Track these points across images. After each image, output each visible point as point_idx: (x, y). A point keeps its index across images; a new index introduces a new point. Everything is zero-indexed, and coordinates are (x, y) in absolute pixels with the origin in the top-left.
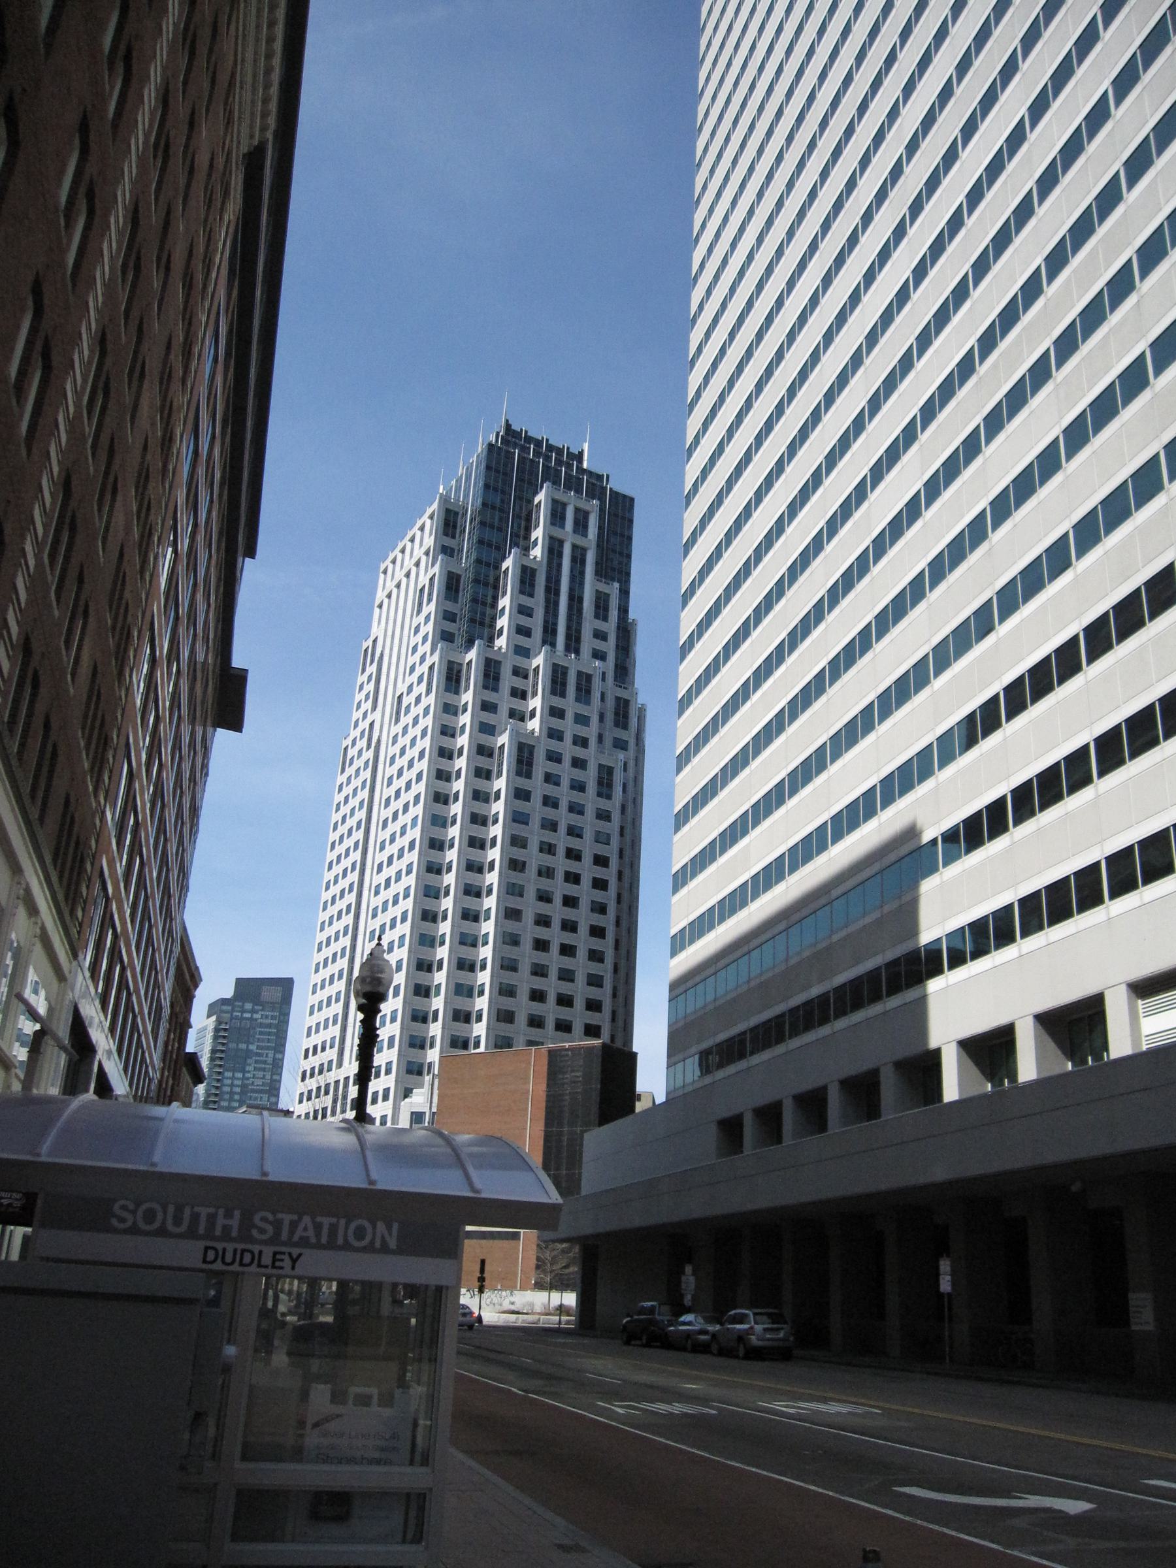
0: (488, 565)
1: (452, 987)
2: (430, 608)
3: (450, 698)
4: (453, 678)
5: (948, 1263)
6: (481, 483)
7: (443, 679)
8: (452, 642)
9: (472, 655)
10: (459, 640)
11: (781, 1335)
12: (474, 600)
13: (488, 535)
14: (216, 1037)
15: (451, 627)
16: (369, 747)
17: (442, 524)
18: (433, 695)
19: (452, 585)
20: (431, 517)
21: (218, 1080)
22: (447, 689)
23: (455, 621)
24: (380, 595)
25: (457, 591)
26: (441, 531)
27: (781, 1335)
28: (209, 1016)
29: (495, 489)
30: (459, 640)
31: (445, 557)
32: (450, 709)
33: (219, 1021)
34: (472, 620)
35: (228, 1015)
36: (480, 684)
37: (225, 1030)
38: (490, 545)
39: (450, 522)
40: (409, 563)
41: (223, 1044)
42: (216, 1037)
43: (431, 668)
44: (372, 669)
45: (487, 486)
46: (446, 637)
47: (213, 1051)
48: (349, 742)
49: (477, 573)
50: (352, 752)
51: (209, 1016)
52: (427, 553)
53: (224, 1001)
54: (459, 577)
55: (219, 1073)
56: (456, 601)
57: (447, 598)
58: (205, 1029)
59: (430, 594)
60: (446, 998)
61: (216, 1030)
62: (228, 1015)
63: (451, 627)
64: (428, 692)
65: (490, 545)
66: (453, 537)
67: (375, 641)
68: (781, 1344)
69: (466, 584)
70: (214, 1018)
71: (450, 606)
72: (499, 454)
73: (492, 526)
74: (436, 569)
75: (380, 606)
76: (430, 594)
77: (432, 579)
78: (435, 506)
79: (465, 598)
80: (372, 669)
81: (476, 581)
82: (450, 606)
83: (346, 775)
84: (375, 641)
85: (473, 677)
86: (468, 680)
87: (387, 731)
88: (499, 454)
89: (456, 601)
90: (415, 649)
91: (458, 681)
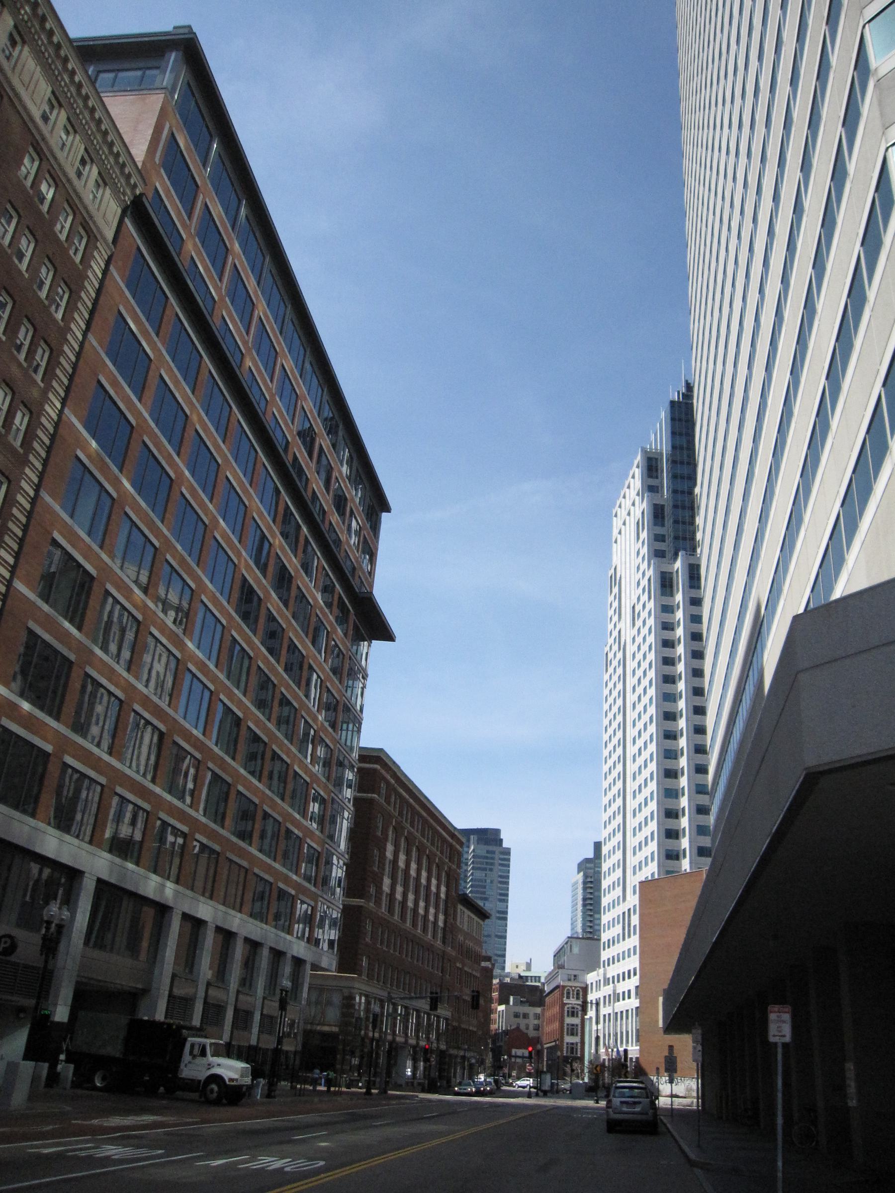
0: (683, 492)
1: (695, 829)
2: (644, 535)
3: (666, 601)
4: (666, 584)
5: (787, 1017)
6: (669, 431)
7: (659, 586)
8: (664, 557)
9: (678, 564)
10: (669, 555)
11: (638, 1109)
12: (676, 522)
13: (680, 470)
14: (585, 889)
15: (661, 546)
16: (619, 649)
17: (645, 471)
18: (652, 600)
19: (657, 514)
20: (638, 467)
21: (591, 921)
22: (663, 594)
23: (664, 541)
24: (615, 532)
25: (663, 518)
26: (645, 475)
27: (638, 1109)
28: (578, 873)
29: (681, 434)
30: (669, 555)
31: (650, 494)
32: (668, 609)
33: (586, 876)
34: (676, 538)
35: (592, 871)
36: (687, 584)
37: (591, 882)
38: (682, 478)
39: (651, 467)
40: (628, 503)
41: (591, 893)
42: (585, 889)
43: (649, 580)
44: (616, 590)
45: (673, 433)
46: (658, 554)
47: (584, 899)
48: (608, 648)
49: (675, 500)
50: (611, 655)
51: (578, 873)
52: (638, 494)
53: (587, 860)
54: (663, 507)
55: (591, 916)
56: (663, 525)
57: (655, 524)
58: (576, 883)
59: (643, 524)
60: (690, 838)
61: (585, 883)
62: (592, 871)
63: (661, 546)
64: (650, 598)
65: (682, 478)
66: (657, 478)
67: (615, 569)
68: (639, 1117)
69: (668, 510)
70: (582, 874)
71: (660, 530)
72: (680, 407)
73: (682, 463)
74: (645, 504)
75: (616, 542)
76: (643, 524)
77: (643, 513)
78: (639, 458)
79: (669, 522)
80: (616, 590)
81: (675, 506)
82: (660, 530)
83: (609, 674)
84: (615, 569)
85: (681, 581)
86: (678, 584)
87: (628, 633)
88: (680, 407)
89: (663, 525)
90: (638, 568)
91: (671, 586)
